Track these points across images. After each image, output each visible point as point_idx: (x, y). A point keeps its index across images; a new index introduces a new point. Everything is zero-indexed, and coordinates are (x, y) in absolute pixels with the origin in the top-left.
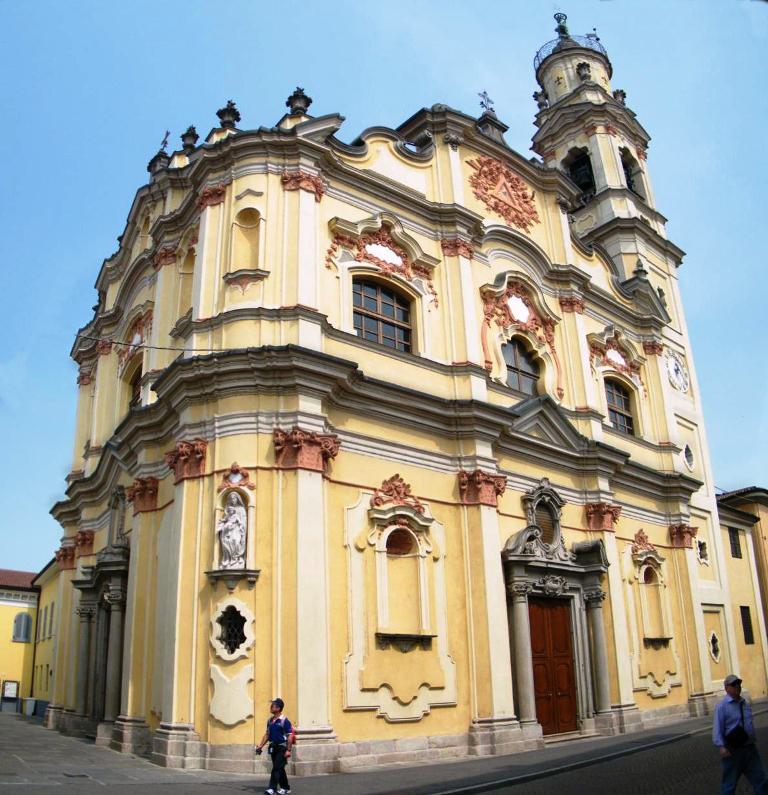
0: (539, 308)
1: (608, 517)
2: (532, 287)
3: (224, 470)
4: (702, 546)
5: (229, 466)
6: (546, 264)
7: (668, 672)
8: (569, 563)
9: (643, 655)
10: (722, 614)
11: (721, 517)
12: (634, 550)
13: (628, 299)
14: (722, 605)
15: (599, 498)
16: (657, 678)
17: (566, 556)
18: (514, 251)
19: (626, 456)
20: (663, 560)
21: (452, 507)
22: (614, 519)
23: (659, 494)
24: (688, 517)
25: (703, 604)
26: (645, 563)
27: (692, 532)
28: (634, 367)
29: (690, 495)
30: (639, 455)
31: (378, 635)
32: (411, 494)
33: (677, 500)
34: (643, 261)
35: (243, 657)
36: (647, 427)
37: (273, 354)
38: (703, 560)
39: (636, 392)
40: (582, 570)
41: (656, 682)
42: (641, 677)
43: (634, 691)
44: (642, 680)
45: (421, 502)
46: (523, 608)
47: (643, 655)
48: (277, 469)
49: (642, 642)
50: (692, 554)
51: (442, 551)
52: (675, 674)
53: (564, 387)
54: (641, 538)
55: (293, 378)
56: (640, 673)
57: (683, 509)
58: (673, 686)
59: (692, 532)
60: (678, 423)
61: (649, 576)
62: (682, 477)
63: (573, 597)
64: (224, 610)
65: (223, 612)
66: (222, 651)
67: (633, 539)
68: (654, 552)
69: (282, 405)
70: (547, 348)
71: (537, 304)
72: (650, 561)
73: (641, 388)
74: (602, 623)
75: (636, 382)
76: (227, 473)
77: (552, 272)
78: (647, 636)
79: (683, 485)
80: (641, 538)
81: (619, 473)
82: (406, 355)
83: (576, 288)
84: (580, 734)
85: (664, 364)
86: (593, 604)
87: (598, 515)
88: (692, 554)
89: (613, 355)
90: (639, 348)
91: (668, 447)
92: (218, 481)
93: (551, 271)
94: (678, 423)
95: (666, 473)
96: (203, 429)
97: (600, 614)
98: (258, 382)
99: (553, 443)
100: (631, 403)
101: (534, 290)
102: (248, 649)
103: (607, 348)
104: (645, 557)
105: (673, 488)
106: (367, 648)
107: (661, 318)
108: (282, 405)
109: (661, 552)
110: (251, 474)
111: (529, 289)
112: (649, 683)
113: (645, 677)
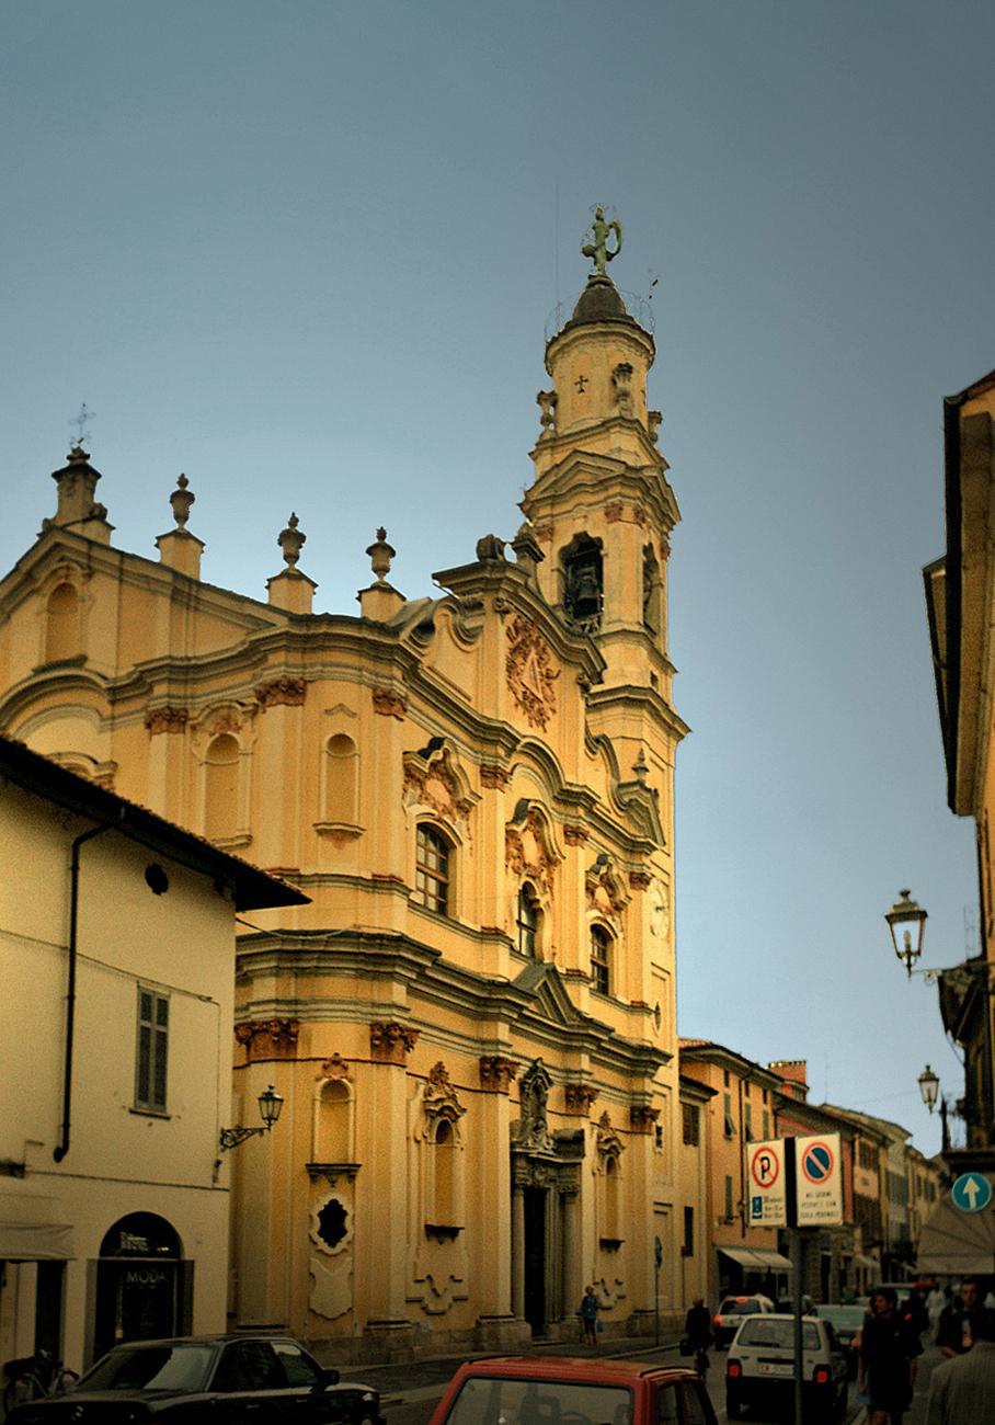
0: (549, 846)
1: (399, 1045)
2: (545, 817)
3: (325, 1059)
4: (659, 1130)
5: (329, 1055)
6: (560, 781)
7: (452, 1277)
8: (551, 1153)
9: (599, 1258)
10: (669, 1216)
11: (681, 1093)
12: (428, 1093)
13: (622, 810)
14: (670, 1205)
15: (580, 1079)
16: (437, 1287)
17: (548, 1144)
18: (536, 768)
19: (434, 954)
20: (623, 1148)
21: (558, 1116)
22: (409, 1046)
23: (625, 1067)
24: (651, 1096)
25: (656, 1203)
26: (440, 1113)
27: (655, 1115)
28: (464, 808)
29: (656, 1070)
30: (458, 952)
31: (426, 1226)
32: (449, 1082)
33: (645, 1074)
34: (647, 754)
35: (344, 1250)
36: (621, 990)
37: (385, 942)
38: (658, 1149)
39: (615, 941)
40: (560, 1161)
41: (434, 1290)
42: (417, 1281)
43: (407, 1302)
44: (418, 1285)
45: (456, 1090)
46: (521, 1201)
47: (599, 1258)
48: (372, 1062)
49: (423, 1228)
50: (649, 1141)
51: (624, 1176)
52: (460, 1281)
53: (557, 945)
54: (438, 1074)
55: (394, 965)
56: (415, 1274)
57: (649, 1086)
58: (456, 1299)
59: (655, 1115)
60: (654, 974)
61: (444, 1133)
62: (654, 1051)
63: (549, 1189)
64: (327, 1203)
65: (326, 1206)
66: (322, 1243)
67: (427, 1075)
68: (453, 1097)
69: (375, 993)
70: (547, 897)
71: (546, 836)
72: (446, 1112)
73: (467, 844)
74: (573, 1216)
75: (463, 835)
76: (327, 1063)
77: (563, 791)
78: (429, 1223)
79: (591, 1032)
80: (438, 1074)
81: (422, 975)
82: (601, 995)
83: (398, 673)
84: (545, 1339)
85: (653, 895)
86: (568, 1199)
87: (578, 1097)
88: (649, 1141)
89: (436, 788)
90: (472, 771)
91: (639, 1007)
92: (317, 1068)
93: (562, 790)
94: (654, 974)
95: (486, 977)
96: (293, 1007)
97: (572, 1209)
98: (360, 966)
99: (549, 1019)
100: (608, 953)
101: (547, 822)
102: (349, 1243)
103: (428, 776)
104: (440, 1105)
105: (643, 1060)
106: (595, 1251)
107: (656, 841)
108: (375, 993)
109: (463, 1099)
110: (350, 1064)
111: (543, 820)
112: (424, 1290)
113: (422, 1281)
